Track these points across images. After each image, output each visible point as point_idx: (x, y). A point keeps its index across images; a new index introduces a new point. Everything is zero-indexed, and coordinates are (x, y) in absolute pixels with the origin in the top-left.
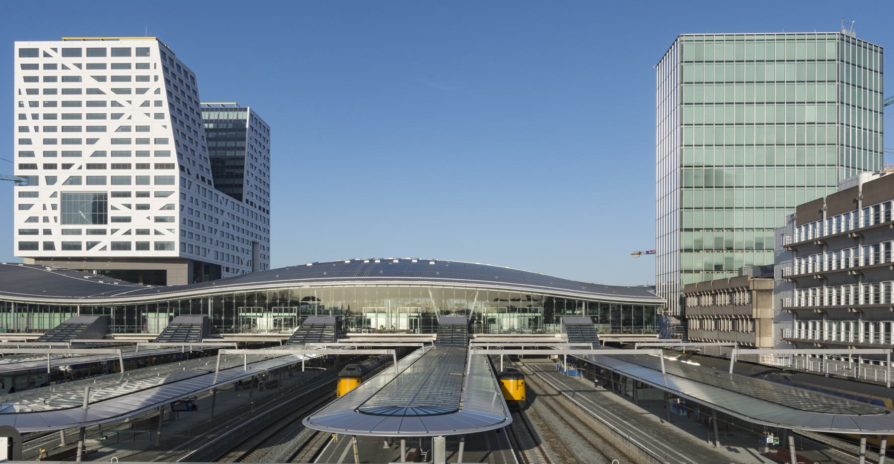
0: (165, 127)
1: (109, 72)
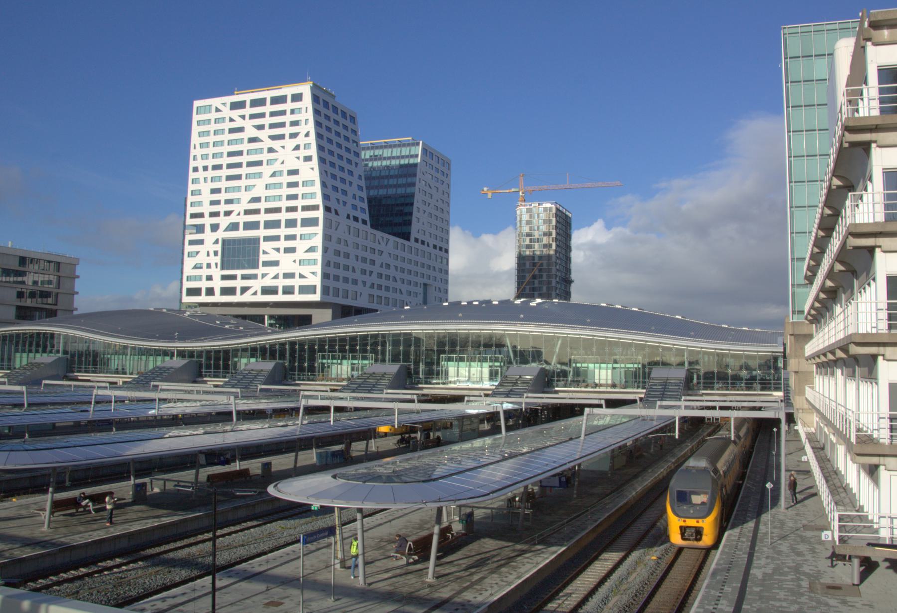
0: (313, 169)
1: (267, 121)
